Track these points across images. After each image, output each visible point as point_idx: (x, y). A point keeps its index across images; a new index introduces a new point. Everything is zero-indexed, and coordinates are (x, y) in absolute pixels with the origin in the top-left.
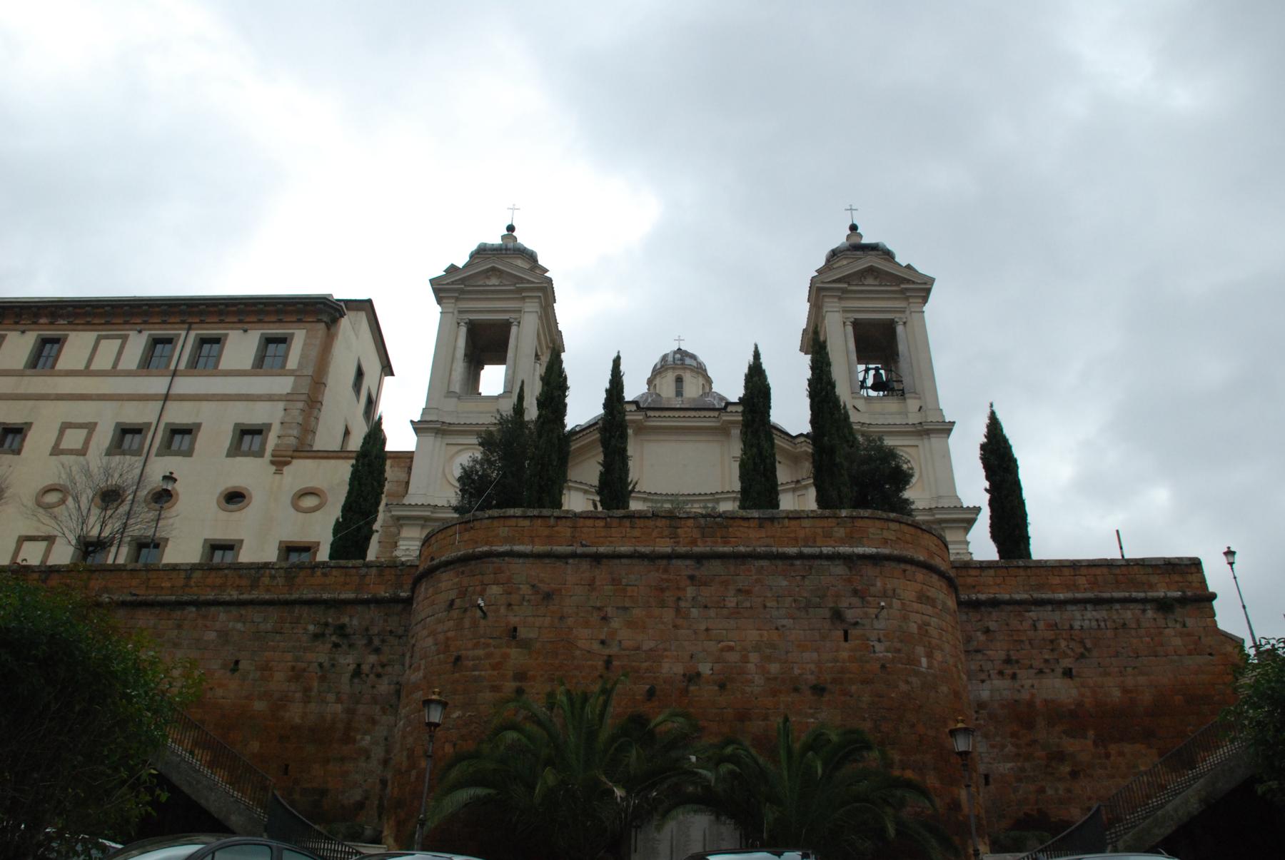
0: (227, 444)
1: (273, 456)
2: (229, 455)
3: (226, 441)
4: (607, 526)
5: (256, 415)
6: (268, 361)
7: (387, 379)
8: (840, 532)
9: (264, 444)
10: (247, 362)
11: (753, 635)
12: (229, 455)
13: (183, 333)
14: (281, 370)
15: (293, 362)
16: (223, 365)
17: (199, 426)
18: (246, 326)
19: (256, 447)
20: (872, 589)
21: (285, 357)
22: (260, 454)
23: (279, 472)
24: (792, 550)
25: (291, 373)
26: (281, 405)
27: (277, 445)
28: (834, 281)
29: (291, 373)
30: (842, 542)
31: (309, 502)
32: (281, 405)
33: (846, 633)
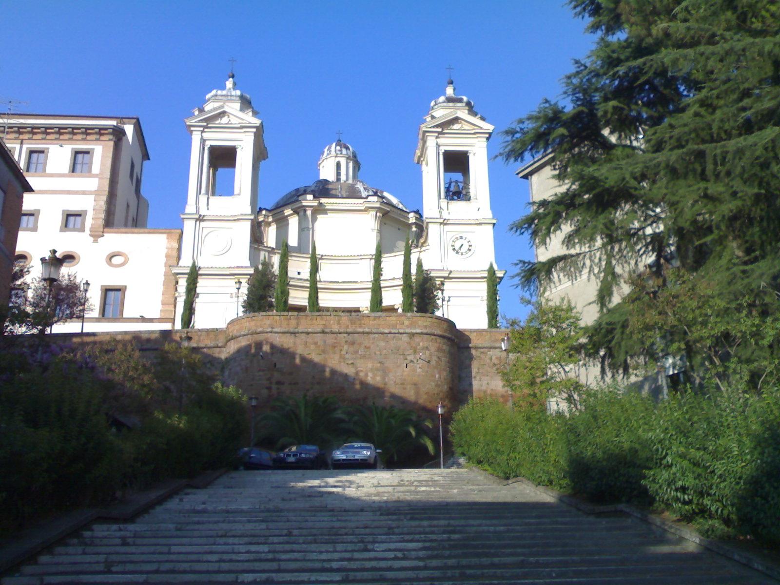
0: (60, 225)
1: (91, 231)
2: (61, 230)
3: (59, 220)
4: (312, 319)
5: (75, 204)
6: (78, 167)
7: (146, 163)
8: (406, 322)
9: (83, 224)
10: (66, 167)
11: (370, 365)
12: (61, 230)
13: (18, 146)
14: (88, 172)
15: (96, 168)
16: (49, 170)
17: (38, 211)
18: (60, 142)
19: (78, 225)
20: (418, 347)
21: (90, 164)
22: (82, 229)
23: (95, 241)
24: (387, 331)
25: (95, 176)
26: (92, 197)
27: (92, 225)
28: (434, 127)
29: (95, 176)
30: (408, 327)
31: (116, 260)
32: (92, 197)
33: (275, 366)
